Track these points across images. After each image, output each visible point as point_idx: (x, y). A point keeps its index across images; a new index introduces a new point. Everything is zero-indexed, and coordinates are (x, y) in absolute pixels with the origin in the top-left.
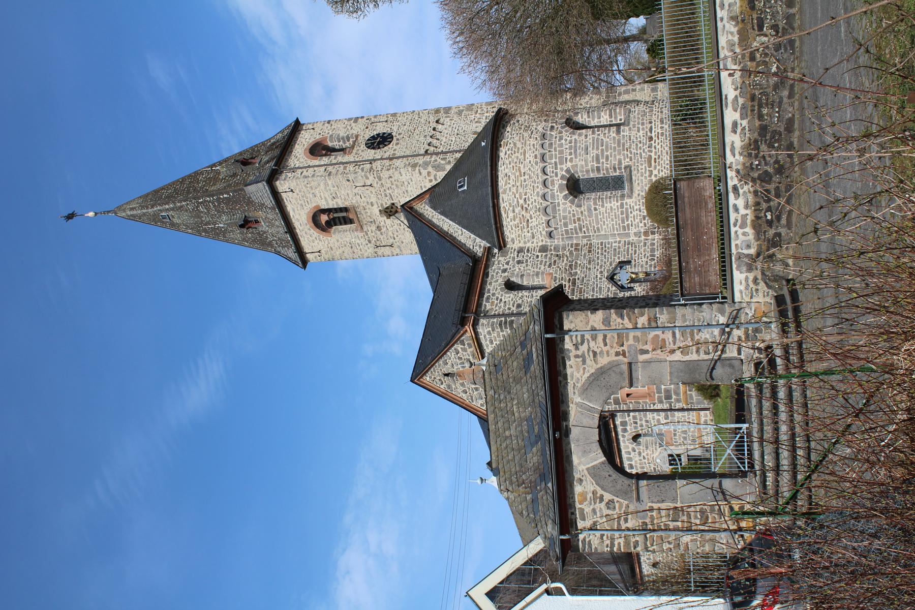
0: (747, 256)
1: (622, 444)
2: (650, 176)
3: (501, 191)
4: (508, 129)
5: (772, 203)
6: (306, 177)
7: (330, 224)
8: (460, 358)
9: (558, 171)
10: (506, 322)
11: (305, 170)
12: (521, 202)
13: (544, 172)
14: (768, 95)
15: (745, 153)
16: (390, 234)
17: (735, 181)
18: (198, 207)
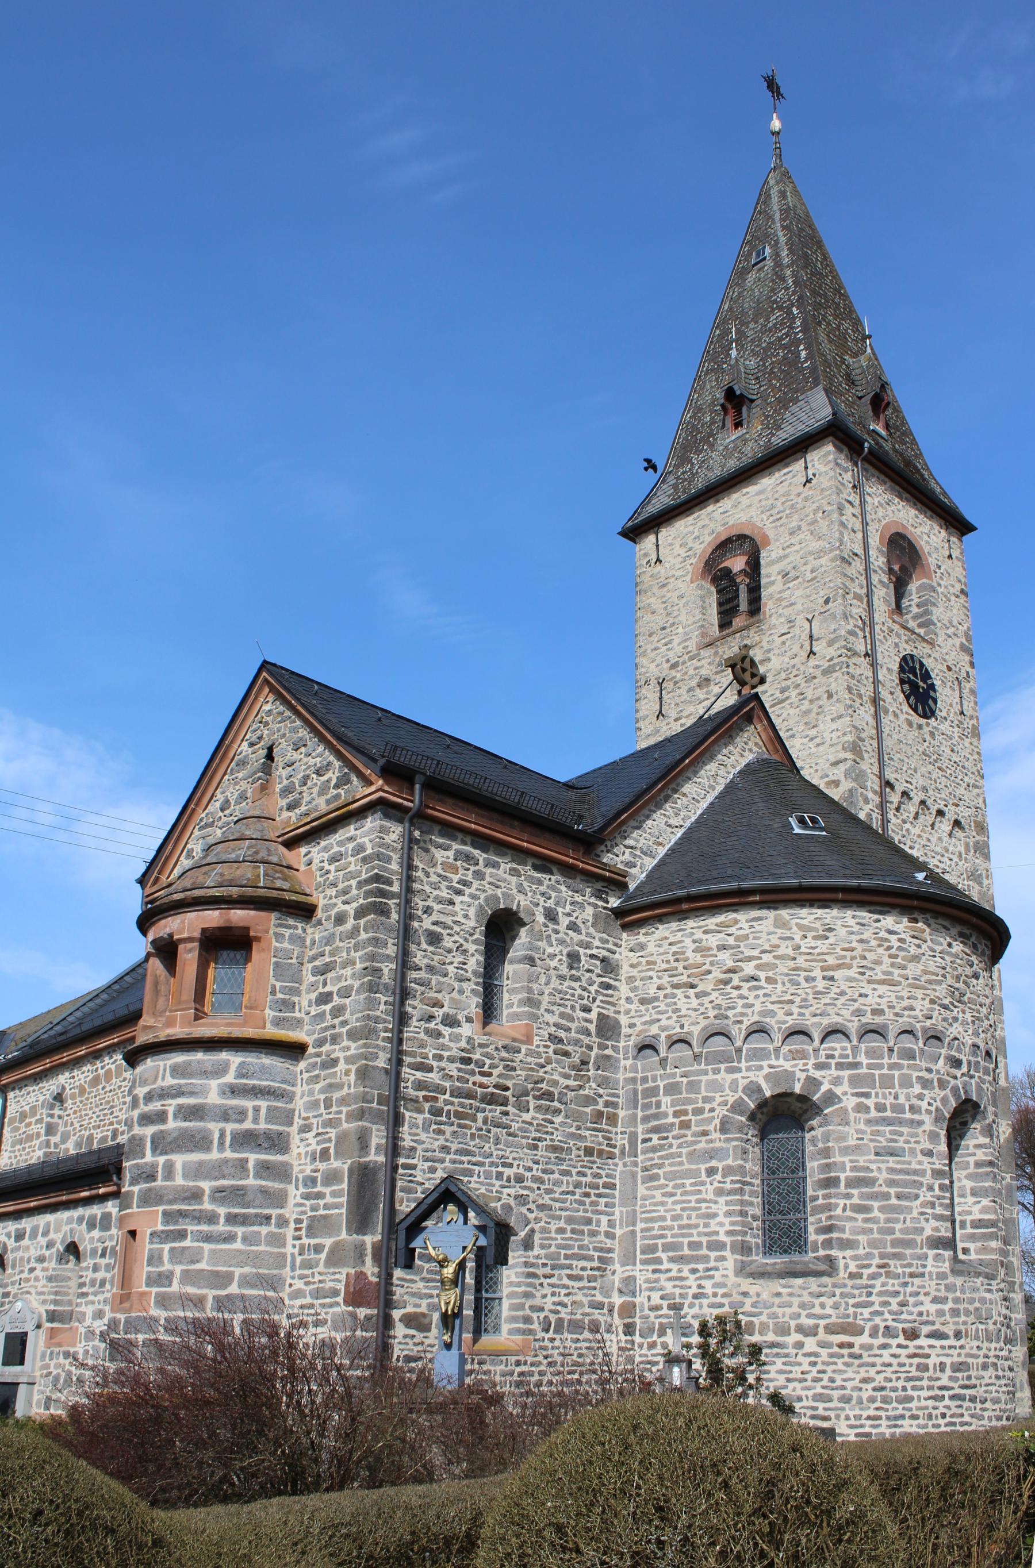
1: (64, 1215)
2: (800, 1329)
3: (785, 913)
4: (958, 947)
6: (841, 508)
7: (722, 580)
9: (833, 1072)
10: (382, 893)
11: (857, 511)
12: (749, 969)
13: (831, 1032)
18: (780, 308)
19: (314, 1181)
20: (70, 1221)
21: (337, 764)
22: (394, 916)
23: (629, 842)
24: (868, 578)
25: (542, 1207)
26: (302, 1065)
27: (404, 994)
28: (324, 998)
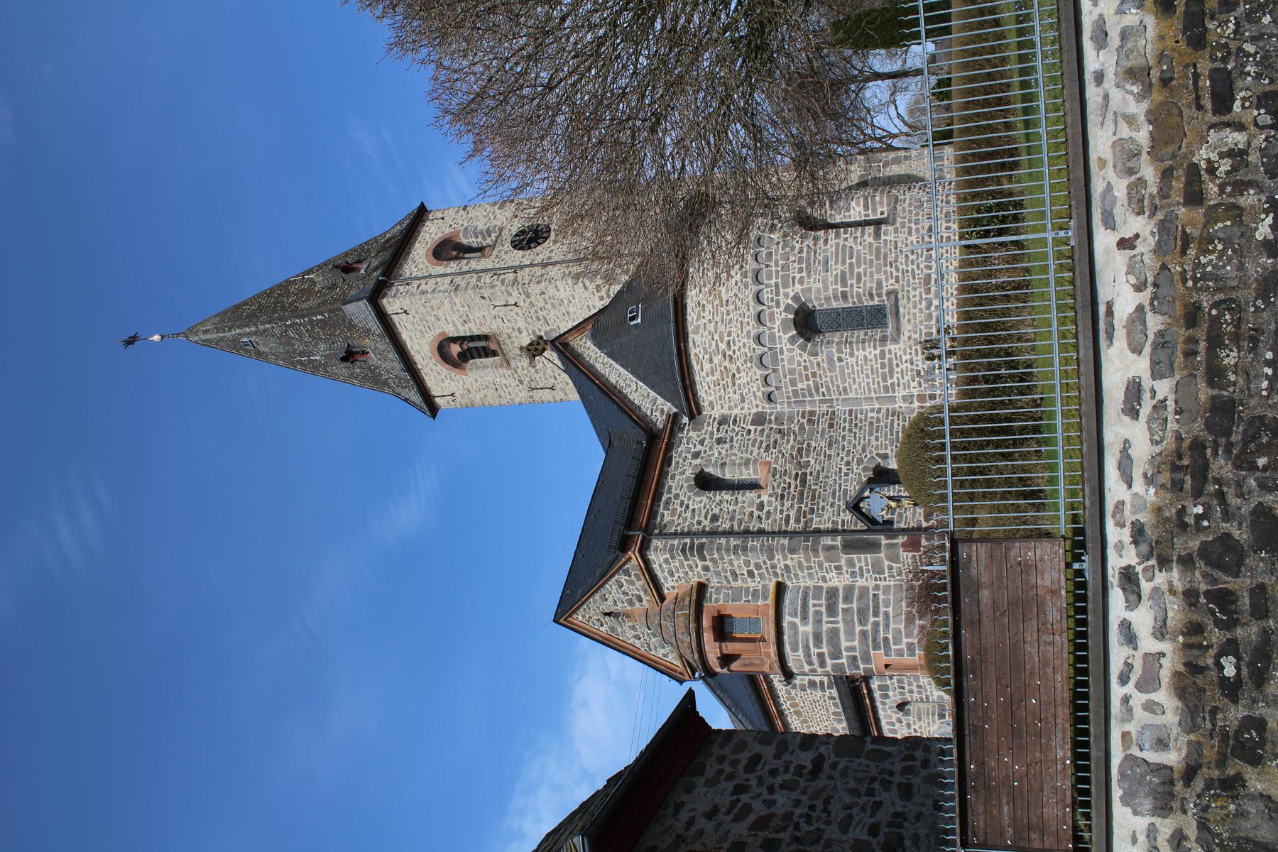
0: (1159, 768)
1: (881, 714)
2: (928, 308)
3: (690, 329)
5: (1239, 632)
6: (423, 293)
7: (465, 356)
8: (625, 593)
9: (781, 298)
10: (692, 547)
11: (423, 282)
12: (723, 346)
13: (758, 300)
14: (1240, 309)
15: (1165, 477)
16: (549, 371)
17: (1130, 557)
18: (286, 331)
19: (853, 573)
20: (884, 710)
21: (617, 576)
22: (704, 540)
23: (649, 413)
24: (466, 273)
25: (864, 450)
26: (788, 583)
27: (747, 532)
28: (751, 574)
